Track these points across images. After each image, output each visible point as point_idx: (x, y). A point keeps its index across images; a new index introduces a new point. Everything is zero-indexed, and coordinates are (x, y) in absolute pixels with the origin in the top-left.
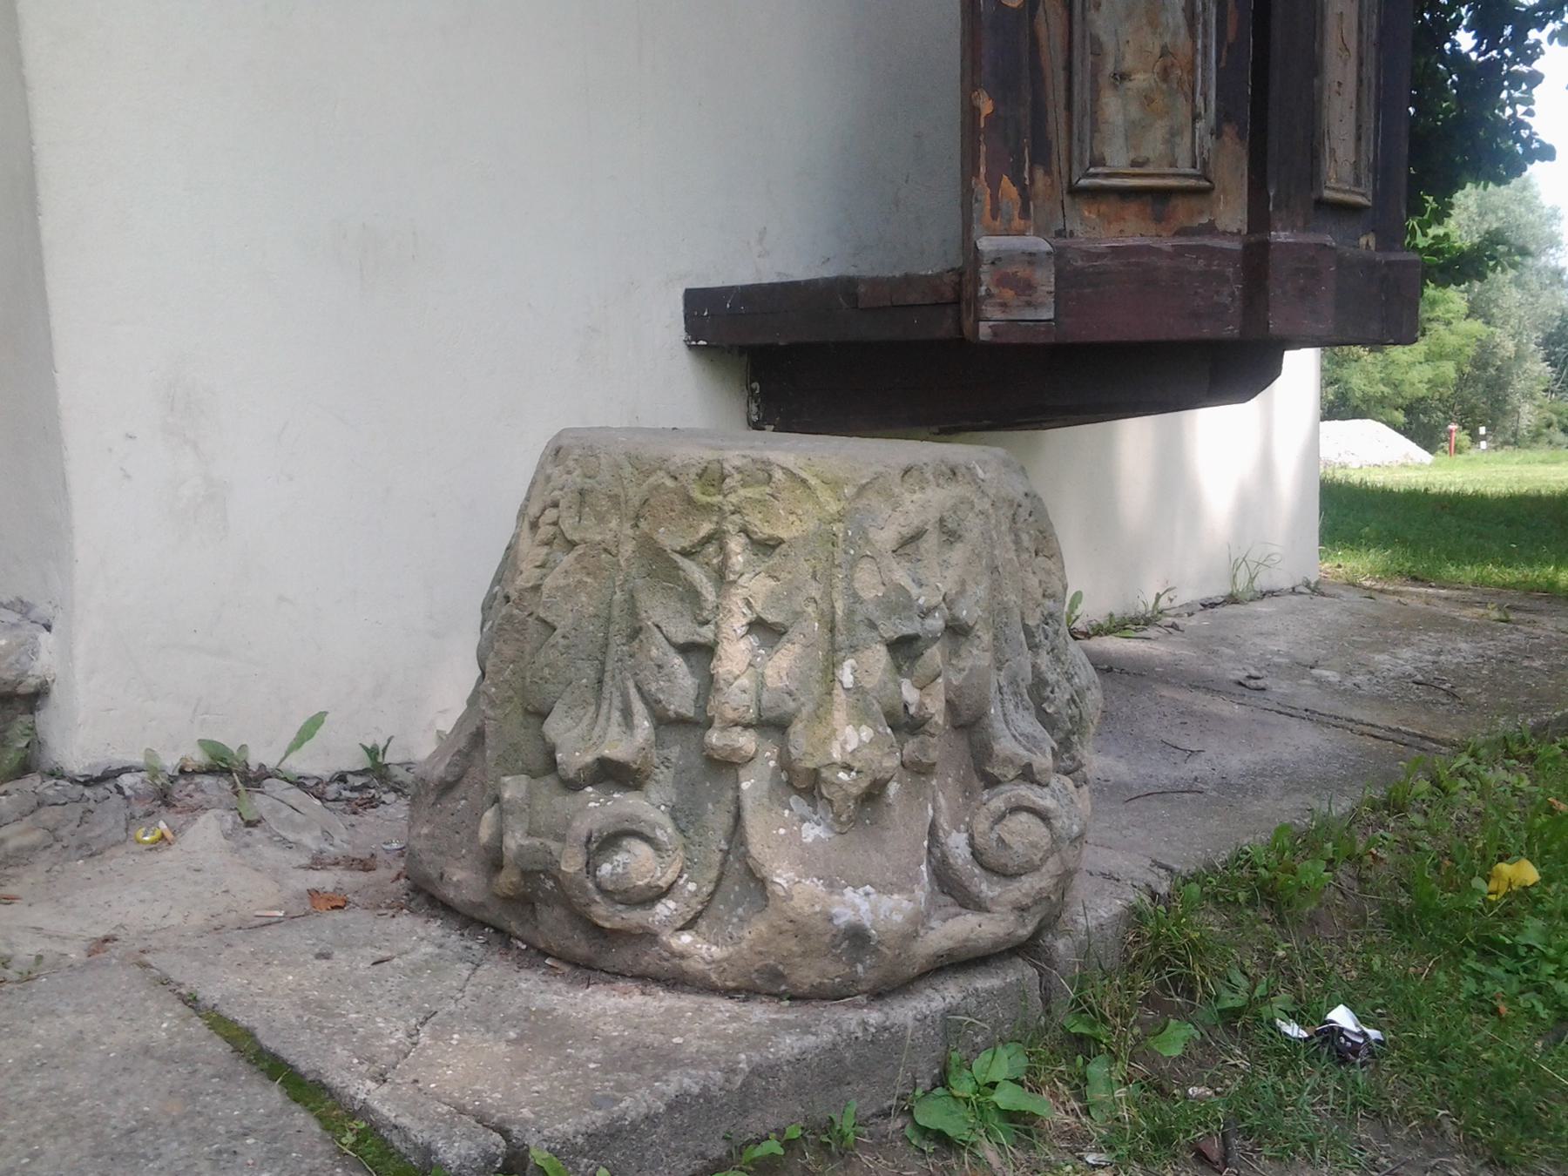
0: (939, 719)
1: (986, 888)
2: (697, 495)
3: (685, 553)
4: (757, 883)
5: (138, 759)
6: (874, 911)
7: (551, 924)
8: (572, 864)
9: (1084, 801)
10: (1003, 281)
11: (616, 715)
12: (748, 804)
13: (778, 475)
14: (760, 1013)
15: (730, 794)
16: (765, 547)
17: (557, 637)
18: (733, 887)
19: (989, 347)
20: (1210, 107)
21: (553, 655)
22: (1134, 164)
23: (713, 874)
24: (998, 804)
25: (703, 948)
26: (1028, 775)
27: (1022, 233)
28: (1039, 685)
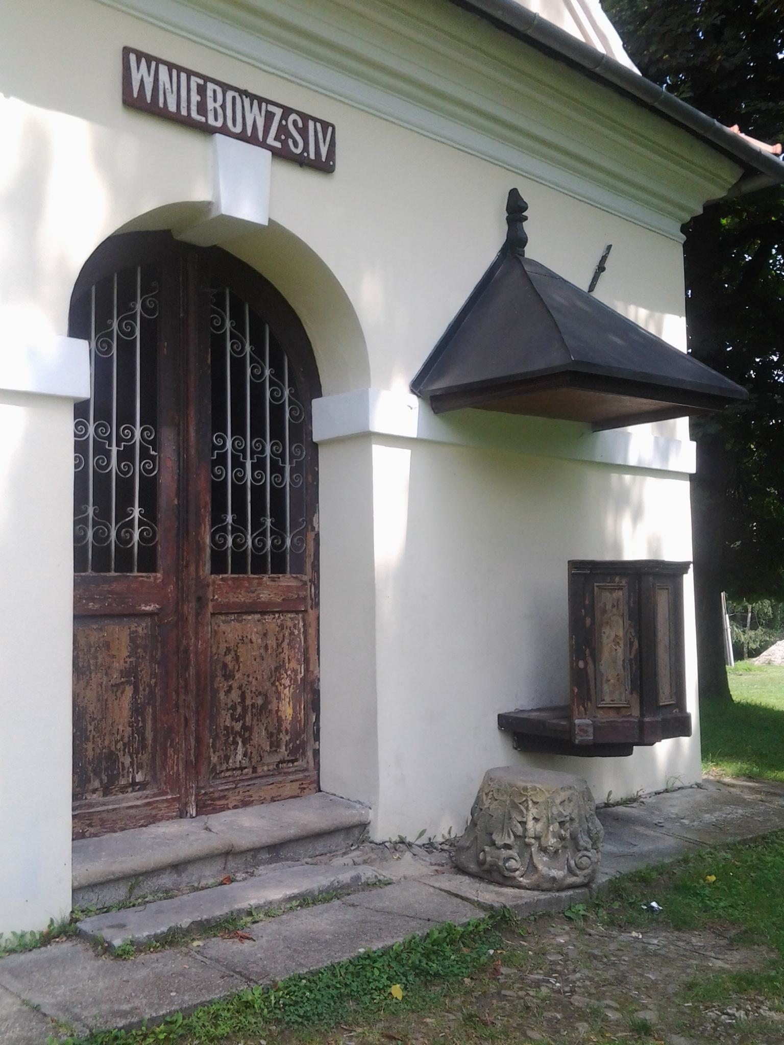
0: (569, 838)
1: (578, 872)
2: (522, 792)
3: (520, 803)
4: (535, 868)
5: (388, 840)
6: (557, 874)
7: (495, 875)
8: (501, 864)
9: (599, 856)
10: (580, 730)
11: (506, 835)
12: (533, 853)
13: (538, 789)
14: (536, 893)
15: (530, 851)
16: (535, 803)
17: (494, 818)
18: (530, 869)
19: (577, 745)
20: (628, 687)
21: (493, 822)
22: (612, 701)
23: (526, 866)
24: (580, 855)
25: (525, 881)
26: (586, 849)
27: (585, 718)
28: (589, 829)
